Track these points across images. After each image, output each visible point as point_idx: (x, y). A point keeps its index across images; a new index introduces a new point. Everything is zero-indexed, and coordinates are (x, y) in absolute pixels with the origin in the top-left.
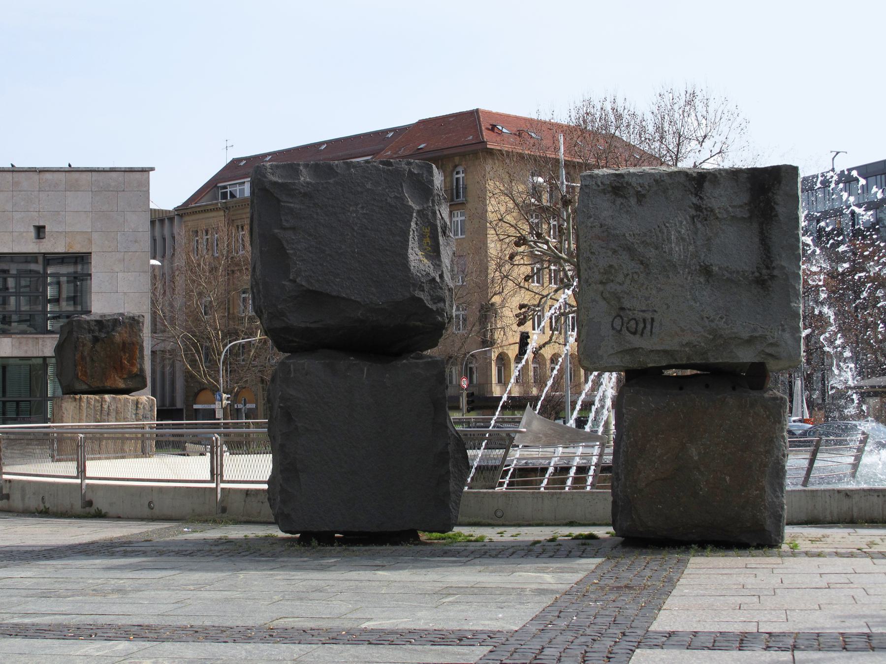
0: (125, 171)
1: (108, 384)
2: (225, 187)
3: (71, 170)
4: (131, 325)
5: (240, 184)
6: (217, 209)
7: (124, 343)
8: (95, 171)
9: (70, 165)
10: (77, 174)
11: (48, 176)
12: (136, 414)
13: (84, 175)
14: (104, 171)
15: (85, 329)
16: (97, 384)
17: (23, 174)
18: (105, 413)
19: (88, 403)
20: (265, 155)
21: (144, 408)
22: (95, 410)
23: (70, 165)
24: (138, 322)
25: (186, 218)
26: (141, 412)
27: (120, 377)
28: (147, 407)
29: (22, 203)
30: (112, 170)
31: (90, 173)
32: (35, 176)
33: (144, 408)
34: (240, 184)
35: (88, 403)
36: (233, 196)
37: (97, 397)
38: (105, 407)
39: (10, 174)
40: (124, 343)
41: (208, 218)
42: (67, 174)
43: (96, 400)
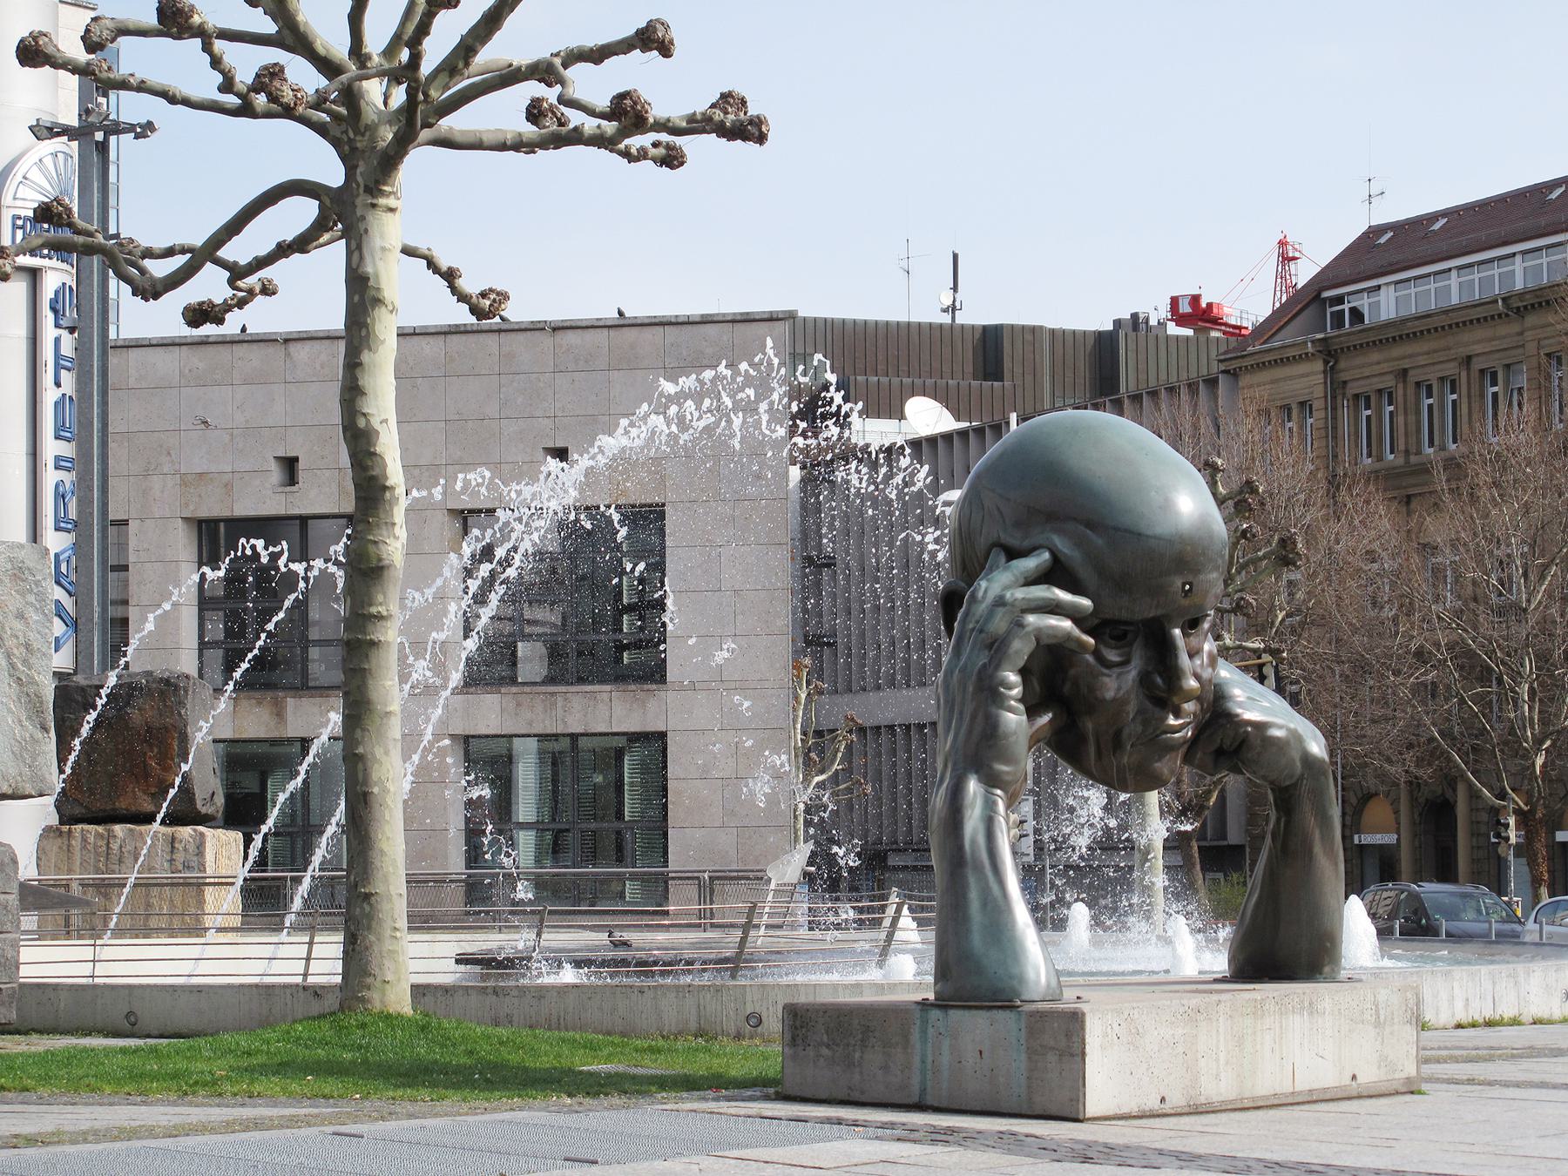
0: (733, 321)
1: (122, 805)
2: (1340, 300)
3: (623, 323)
4: (162, 693)
5: (1370, 290)
6: (1306, 357)
7: (149, 730)
8: (670, 324)
9: (621, 313)
10: (634, 330)
11: (571, 337)
12: (171, 861)
13: (648, 333)
14: (688, 322)
15: (77, 702)
16: (99, 805)
17: (521, 336)
18: (114, 858)
19: (84, 840)
20: (1434, 217)
21: (185, 850)
22: (97, 854)
23: (621, 313)
24: (177, 687)
25: (1245, 380)
26: (180, 857)
27: (144, 792)
28: (192, 848)
29: (520, 400)
30: (706, 320)
31: (660, 329)
32: (546, 340)
33: (185, 850)
34: (1370, 290)
35: (84, 840)
36: (1357, 315)
37: (100, 829)
38: (115, 846)
39: (495, 336)
40: (149, 730)
41: (1291, 378)
42: (613, 332)
43: (98, 835)
